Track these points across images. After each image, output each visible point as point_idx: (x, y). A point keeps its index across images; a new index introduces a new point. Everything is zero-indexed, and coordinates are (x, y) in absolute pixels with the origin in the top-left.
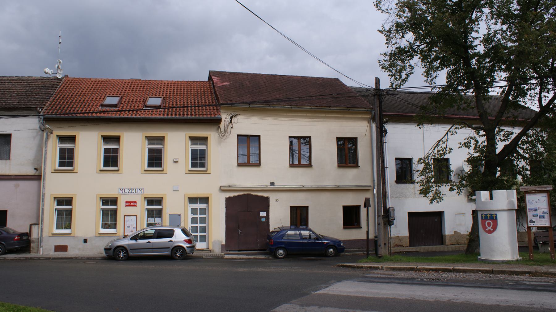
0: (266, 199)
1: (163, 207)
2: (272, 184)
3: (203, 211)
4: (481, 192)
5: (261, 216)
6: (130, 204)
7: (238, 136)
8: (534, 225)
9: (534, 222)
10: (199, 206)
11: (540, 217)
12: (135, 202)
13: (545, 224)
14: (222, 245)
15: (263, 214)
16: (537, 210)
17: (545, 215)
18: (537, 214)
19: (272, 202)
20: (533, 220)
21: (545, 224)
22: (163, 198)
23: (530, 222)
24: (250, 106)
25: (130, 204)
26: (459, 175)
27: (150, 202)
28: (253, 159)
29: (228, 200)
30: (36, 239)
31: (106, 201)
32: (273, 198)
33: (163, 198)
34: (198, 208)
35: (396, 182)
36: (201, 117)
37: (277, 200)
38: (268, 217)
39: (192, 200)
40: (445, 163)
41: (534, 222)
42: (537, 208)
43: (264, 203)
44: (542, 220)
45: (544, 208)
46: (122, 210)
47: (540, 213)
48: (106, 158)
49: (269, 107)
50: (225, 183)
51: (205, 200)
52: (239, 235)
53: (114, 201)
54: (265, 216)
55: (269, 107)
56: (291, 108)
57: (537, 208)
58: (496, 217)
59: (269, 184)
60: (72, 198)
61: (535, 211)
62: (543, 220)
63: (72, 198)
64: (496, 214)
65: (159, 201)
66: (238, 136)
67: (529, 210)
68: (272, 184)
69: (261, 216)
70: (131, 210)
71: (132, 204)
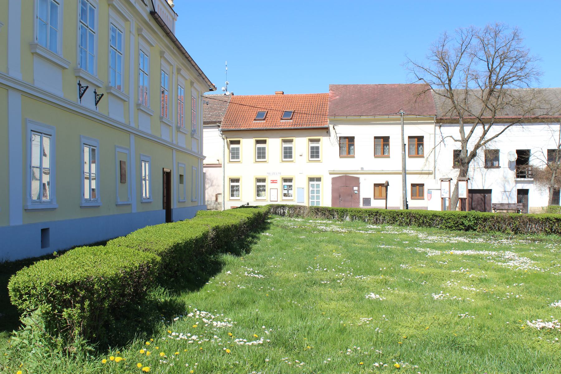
0: (358, 179)
1: (256, 184)
2: (362, 168)
3: (318, 186)
4: (21, 224)
6: (273, 182)
7: (375, 138)
10: (315, 183)
12: (276, 181)
15: (356, 188)
19: (361, 181)
22: (230, 178)
25: (273, 182)
26: (538, 74)
27: (285, 180)
29: (333, 179)
30: (547, 168)
31: (259, 180)
32: (362, 178)
33: (230, 178)
34: (315, 184)
36: (288, 110)
37: (365, 179)
38: (359, 190)
39: (311, 179)
43: (356, 181)
46: (268, 184)
48: (291, 153)
51: (319, 179)
53: (264, 180)
59: (360, 169)
60: (309, 178)
63: (309, 178)
65: (290, 180)
68: (362, 168)
70: (274, 186)
71: (275, 182)
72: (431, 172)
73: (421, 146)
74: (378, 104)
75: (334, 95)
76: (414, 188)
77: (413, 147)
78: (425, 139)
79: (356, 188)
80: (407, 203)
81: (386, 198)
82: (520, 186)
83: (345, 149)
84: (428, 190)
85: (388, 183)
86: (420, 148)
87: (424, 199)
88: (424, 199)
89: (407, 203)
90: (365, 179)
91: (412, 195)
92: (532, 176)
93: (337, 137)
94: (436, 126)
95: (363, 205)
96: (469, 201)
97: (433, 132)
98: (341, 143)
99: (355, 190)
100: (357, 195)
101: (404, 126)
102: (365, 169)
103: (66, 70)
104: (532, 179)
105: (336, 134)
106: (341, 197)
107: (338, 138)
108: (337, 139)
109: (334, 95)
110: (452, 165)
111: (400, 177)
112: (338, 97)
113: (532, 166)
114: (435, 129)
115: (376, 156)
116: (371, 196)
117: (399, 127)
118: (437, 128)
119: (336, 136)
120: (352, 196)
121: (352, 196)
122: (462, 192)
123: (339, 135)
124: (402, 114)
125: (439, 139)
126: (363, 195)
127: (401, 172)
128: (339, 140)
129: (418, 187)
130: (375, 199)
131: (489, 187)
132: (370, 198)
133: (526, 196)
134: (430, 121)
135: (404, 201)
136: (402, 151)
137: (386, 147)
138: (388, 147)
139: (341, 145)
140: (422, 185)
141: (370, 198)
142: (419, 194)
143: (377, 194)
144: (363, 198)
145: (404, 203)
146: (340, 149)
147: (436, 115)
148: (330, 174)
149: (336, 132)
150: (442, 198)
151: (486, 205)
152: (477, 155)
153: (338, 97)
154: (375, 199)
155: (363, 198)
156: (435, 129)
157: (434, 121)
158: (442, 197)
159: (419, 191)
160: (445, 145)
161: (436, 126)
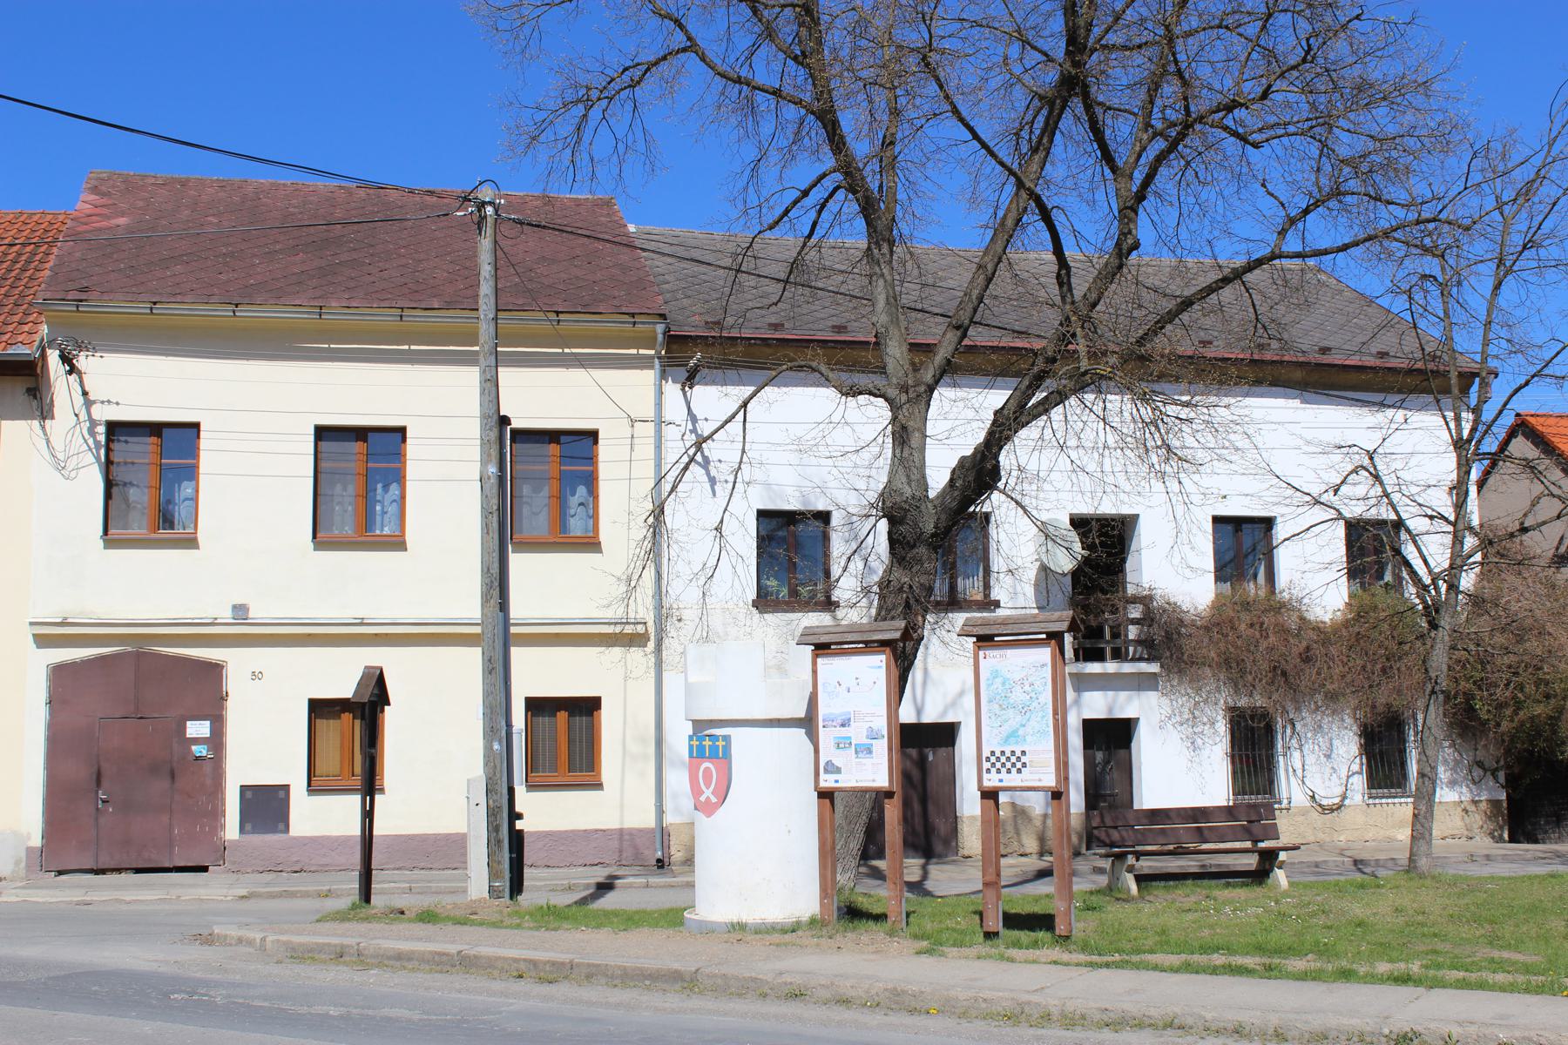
5: (188, 736)
7: (322, 433)
8: (837, 781)
9: (838, 770)
11: (856, 752)
13: (1040, 780)
14: (29, 850)
15: (198, 729)
16: (849, 720)
17: (874, 742)
18: (850, 738)
19: (235, 683)
20: (837, 762)
21: (874, 781)
23: (826, 771)
24: (78, 306)
28: (576, 526)
29: (59, 673)
32: (237, 664)
35: (755, 604)
37: (256, 676)
38: (217, 741)
40: (817, 525)
41: (838, 770)
42: (850, 713)
44: (864, 761)
45: (873, 715)
47: (857, 733)
49: (628, 323)
50: (49, 611)
52: (98, 809)
54: (208, 735)
55: (628, 323)
56: (634, 323)
57: (850, 713)
58: (727, 748)
59: (226, 614)
61: (843, 725)
62: (867, 761)
64: (727, 738)
66: (322, 433)
67: (824, 720)
68: (240, 610)
69: (188, 736)
72: (640, 629)
73: (582, 490)
74: (345, 257)
75: (105, 211)
76: (543, 721)
77: (537, 490)
78: (605, 451)
79: (198, 729)
80: (519, 825)
81: (370, 786)
82: (1097, 705)
83: (140, 497)
84: (700, 725)
85: (380, 681)
86: (574, 501)
87: (598, 786)
88: (598, 786)
89: (519, 825)
90: (256, 676)
91: (531, 765)
92: (1150, 649)
93: (93, 423)
94: (663, 376)
95: (242, 830)
96: (906, 804)
97: (650, 413)
98: (116, 458)
99: (196, 741)
100: (207, 768)
101: (500, 369)
102: (255, 613)
103: (927, 900)
104: (1154, 668)
105: (88, 403)
106: (106, 783)
107: (101, 429)
108: (92, 432)
109: (105, 211)
110: (752, 594)
111: (471, 660)
112: (122, 221)
113: (1145, 600)
114: (660, 393)
115: (322, 536)
116: (296, 779)
117: (470, 377)
118: (672, 390)
119: (83, 416)
120: (173, 776)
121: (173, 776)
122: (1012, 735)
123: (104, 414)
124: (489, 210)
125: (676, 446)
126: (242, 769)
127: (478, 630)
128: (102, 438)
129: (562, 716)
130: (312, 789)
131: (945, 712)
132: (286, 788)
133: (1122, 752)
134: (634, 351)
135: (492, 813)
136: (484, 463)
137: (386, 488)
138: (394, 490)
139: (119, 474)
140: (588, 707)
141: (286, 788)
142: (581, 764)
143: (330, 760)
144: (244, 789)
145: (493, 828)
146: (108, 496)
147: (663, 316)
148: (43, 641)
149: (85, 393)
150: (826, 795)
151: (931, 808)
152: (1001, 485)
153: (122, 221)
154: (312, 789)
155: (244, 789)
156: (660, 393)
157: (652, 352)
158: (827, 782)
159: (570, 741)
160: (713, 481)
161: (663, 376)
